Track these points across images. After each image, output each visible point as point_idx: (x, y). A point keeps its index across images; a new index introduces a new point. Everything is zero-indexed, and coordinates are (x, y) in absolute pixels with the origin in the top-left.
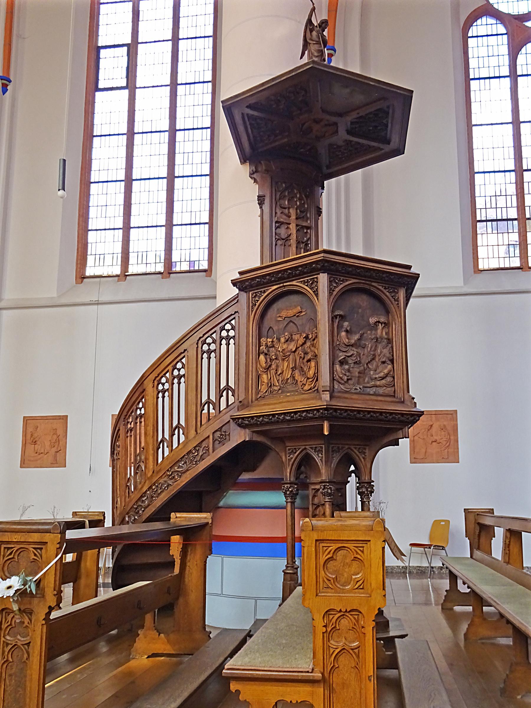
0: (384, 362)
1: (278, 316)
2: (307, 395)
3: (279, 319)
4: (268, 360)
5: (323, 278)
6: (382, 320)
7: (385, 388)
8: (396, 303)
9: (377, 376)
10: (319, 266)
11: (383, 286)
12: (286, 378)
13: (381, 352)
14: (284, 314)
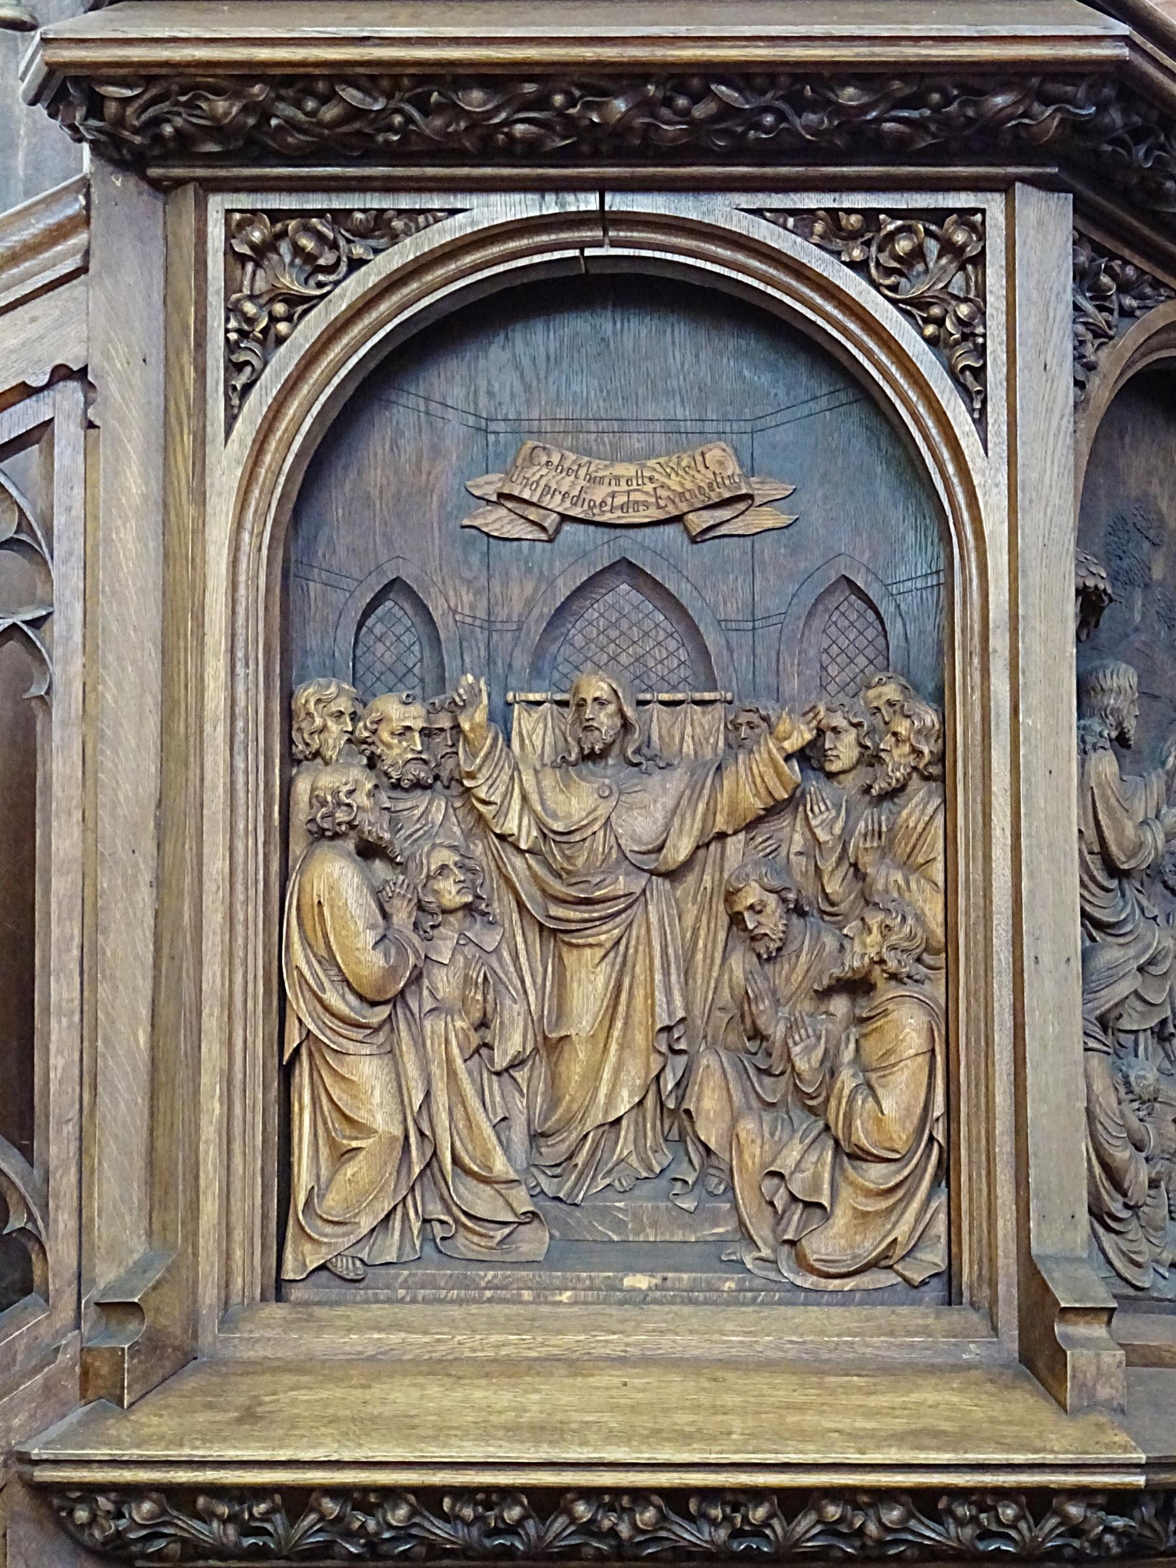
1: (489, 484)
2: (839, 1316)
3: (498, 521)
4: (402, 916)
5: (1033, 240)
10: (1048, 118)
12: (597, 1116)
14: (554, 481)
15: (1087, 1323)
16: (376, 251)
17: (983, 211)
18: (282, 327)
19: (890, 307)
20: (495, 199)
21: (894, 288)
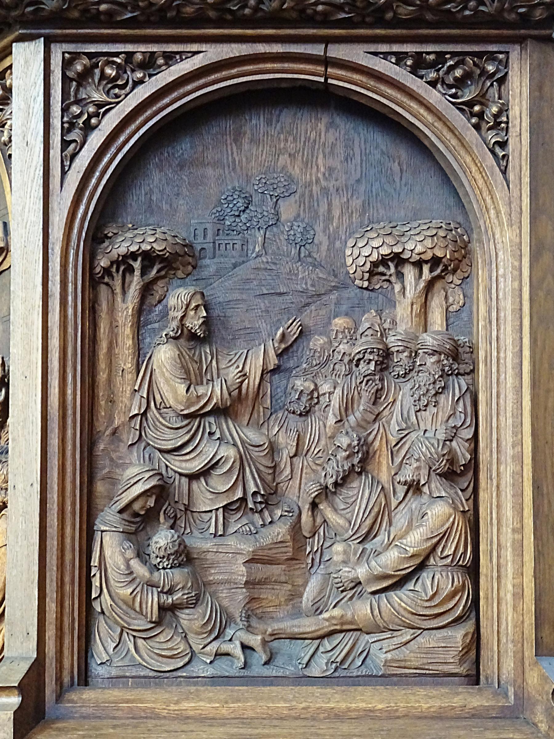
0: (414, 488)
6: (415, 246)
7: (407, 635)
8: (492, 137)
9: (361, 572)
11: (400, 58)
13: (406, 430)
15: (7, 695)
16: (150, 76)
19: (452, 106)
20: (234, 46)
21: (454, 96)
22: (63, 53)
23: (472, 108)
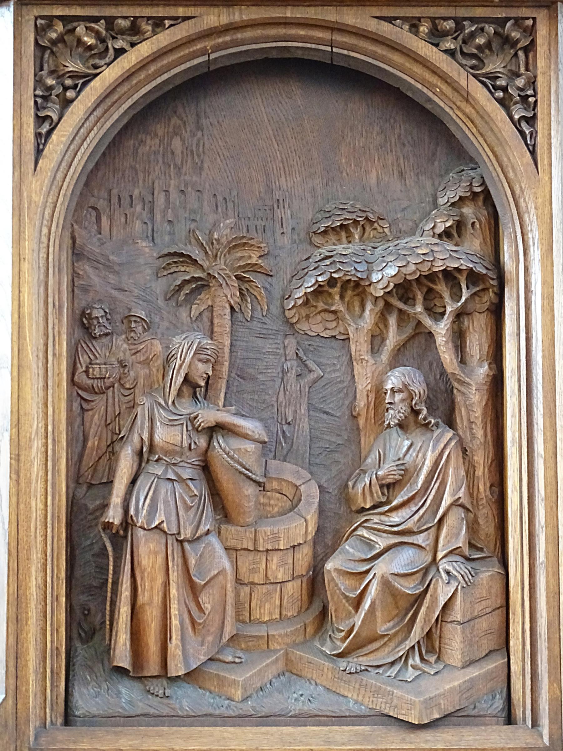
16: (133, 45)
17: (534, 19)
18: (70, 94)
22: (36, 18)
23: (494, 82)
